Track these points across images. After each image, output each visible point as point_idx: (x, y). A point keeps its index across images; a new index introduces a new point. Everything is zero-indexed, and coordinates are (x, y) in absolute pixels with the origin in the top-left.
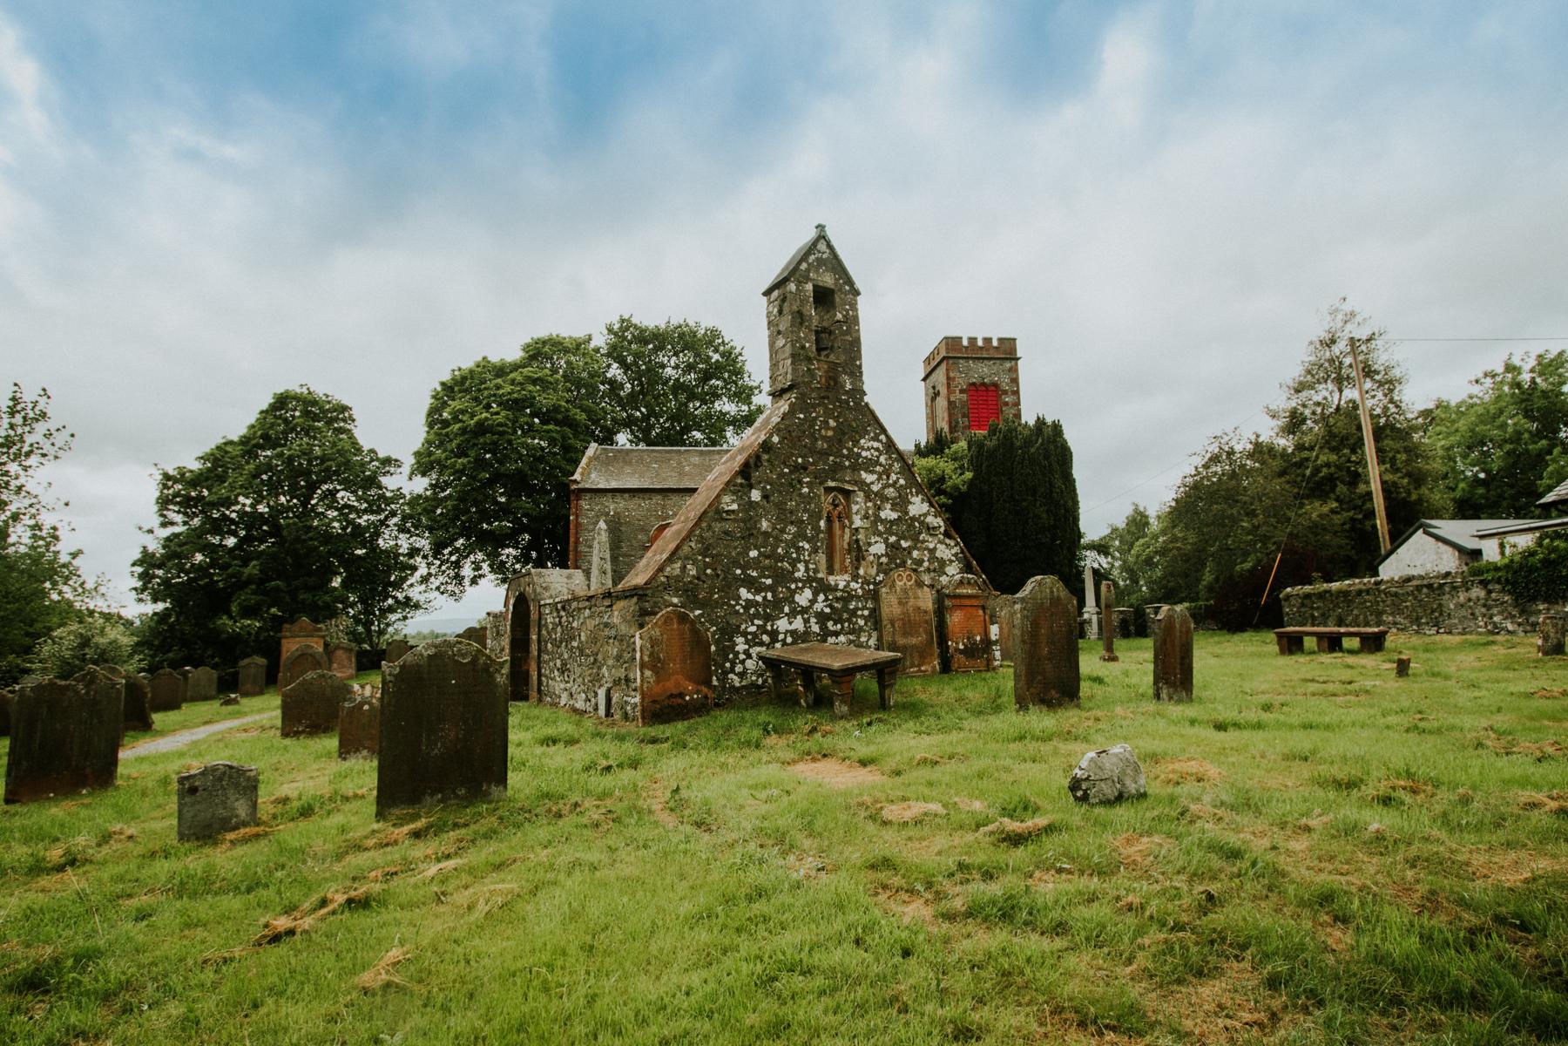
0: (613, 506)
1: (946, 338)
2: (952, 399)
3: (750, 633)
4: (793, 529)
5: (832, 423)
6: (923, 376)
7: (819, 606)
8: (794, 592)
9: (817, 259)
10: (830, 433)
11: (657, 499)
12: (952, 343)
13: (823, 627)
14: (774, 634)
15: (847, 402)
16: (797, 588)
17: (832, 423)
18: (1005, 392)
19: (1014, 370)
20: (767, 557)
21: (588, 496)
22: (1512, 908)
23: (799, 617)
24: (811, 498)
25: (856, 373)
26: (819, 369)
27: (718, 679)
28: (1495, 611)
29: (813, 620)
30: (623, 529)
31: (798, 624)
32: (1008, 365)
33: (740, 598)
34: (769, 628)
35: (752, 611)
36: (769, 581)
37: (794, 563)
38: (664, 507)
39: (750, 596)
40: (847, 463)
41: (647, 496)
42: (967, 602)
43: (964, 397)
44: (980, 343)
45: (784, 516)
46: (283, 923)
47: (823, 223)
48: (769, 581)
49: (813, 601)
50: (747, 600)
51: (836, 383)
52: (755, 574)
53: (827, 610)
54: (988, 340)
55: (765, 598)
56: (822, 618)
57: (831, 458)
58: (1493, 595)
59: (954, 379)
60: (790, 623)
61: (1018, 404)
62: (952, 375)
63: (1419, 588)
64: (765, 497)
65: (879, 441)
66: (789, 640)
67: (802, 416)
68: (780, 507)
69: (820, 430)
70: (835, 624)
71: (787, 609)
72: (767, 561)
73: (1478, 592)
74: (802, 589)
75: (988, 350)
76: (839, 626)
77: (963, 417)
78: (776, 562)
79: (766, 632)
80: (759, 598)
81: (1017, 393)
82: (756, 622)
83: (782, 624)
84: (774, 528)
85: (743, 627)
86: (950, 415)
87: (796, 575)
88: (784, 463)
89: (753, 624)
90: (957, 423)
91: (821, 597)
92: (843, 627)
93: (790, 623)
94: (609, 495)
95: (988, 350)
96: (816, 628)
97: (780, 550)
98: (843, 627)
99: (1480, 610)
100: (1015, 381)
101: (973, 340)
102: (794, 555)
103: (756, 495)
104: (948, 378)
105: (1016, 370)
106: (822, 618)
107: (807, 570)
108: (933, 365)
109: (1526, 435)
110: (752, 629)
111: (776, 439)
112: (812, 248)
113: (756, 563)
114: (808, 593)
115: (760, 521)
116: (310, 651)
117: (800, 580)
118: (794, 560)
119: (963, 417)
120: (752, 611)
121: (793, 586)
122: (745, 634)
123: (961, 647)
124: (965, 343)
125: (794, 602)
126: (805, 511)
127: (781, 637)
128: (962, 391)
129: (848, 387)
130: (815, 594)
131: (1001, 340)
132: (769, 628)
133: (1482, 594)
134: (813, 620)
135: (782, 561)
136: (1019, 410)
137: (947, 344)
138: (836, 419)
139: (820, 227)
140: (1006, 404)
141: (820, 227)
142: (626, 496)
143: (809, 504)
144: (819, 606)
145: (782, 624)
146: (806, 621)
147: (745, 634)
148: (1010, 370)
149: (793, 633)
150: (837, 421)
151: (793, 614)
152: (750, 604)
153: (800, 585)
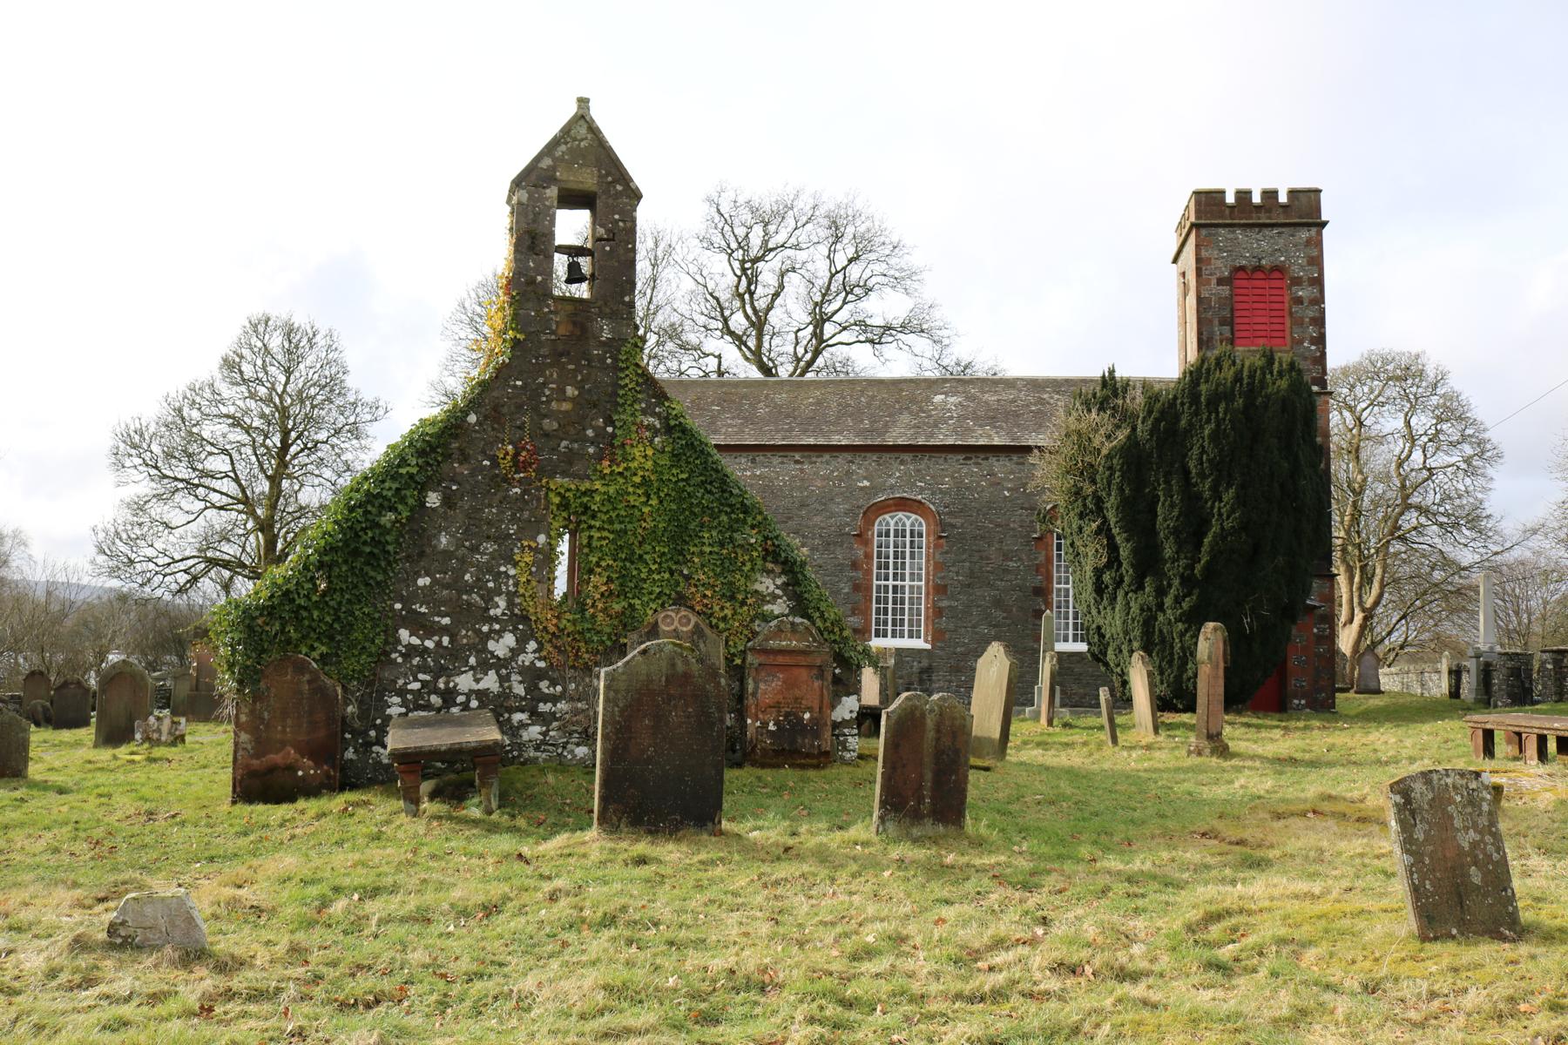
2: (1205, 294)
3: (411, 691)
4: (490, 547)
5: (570, 391)
7: (526, 659)
8: (488, 636)
9: (570, 150)
10: (566, 406)
13: (532, 688)
14: (449, 696)
15: (602, 359)
16: (491, 631)
17: (570, 391)
18: (1297, 281)
20: (447, 586)
23: (492, 673)
24: (526, 502)
26: (555, 313)
27: (356, 751)
29: (515, 677)
31: (490, 682)
32: (1304, 234)
33: (398, 641)
34: (442, 686)
35: (416, 661)
36: (446, 621)
37: (488, 597)
39: (415, 641)
40: (591, 450)
42: (780, 659)
43: (1225, 290)
44: (1256, 199)
45: (475, 530)
47: (585, 95)
48: (446, 621)
49: (515, 652)
50: (409, 646)
51: (584, 329)
52: (423, 610)
53: (541, 664)
54: (1270, 195)
55: (439, 644)
56: (532, 676)
57: (564, 443)
59: (1208, 261)
60: (477, 681)
61: (1319, 300)
64: (448, 501)
65: (654, 414)
66: (474, 704)
67: (519, 383)
68: (473, 516)
69: (549, 402)
70: (553, 683)
71: (472, 661)
72: (445, 592)
74: (500, 633)
75: (1269, 211)
76: (559, 688)
77: (1222, 323)
78: (460, 593)
79: (436, 691)
80: (429, 644)
81: (1319, 282)
82: (421, 676)
83: (465, 682)
84: (460, 545)
85: (401, 682)
87: (492, 612)
88: (483, 452)
89: (416, 679)
90: (1212, 333)
91: (532, 645)
92: (565, 689)
93: (477, 681)
95: (1269, 211)
96: (519, 690)
97: (467, 577)
98: (565, 689)
100: (1317, 262)
101: (1244, 196)
102: (491, 585)
103: (433, 500)
105: (1319, 244)
106: (532, 676)
107: (511, 605)
110: (416, 686)
111: (472, 418)
112: (566, 131)
113: (427, 595)
114: (509, 640)
115: (436, 536)
116: (128, 669)
117: (496, 619)
118: (489, 590)
119: (1222, 323)
120: (416, 661)
121: (485, 629)
122: (402, 692)
123: (772, 727)
124: (1230, 199)
125: (485, 650)
126: (513, 519)
127: (461, 699)
128: (1220, 282)
129: (606, 335)
130: (522, 642)
132: (442, 686)
134: (515, 677)
135: (469, 593)
136: (1323, 312)
138: (579, 386)
139: (583, 102)
140: (1299, 301)
141: (583, 102)
143: (522, 510)
144: (526, 659)
145: (465, 682)
146: (503, 679)
147: (402, 692)
148: (1308, 242)
149: (482, 695)
150: (580, 388)
151: (484, 666)
152: (411, 651)
153: (497, 627)
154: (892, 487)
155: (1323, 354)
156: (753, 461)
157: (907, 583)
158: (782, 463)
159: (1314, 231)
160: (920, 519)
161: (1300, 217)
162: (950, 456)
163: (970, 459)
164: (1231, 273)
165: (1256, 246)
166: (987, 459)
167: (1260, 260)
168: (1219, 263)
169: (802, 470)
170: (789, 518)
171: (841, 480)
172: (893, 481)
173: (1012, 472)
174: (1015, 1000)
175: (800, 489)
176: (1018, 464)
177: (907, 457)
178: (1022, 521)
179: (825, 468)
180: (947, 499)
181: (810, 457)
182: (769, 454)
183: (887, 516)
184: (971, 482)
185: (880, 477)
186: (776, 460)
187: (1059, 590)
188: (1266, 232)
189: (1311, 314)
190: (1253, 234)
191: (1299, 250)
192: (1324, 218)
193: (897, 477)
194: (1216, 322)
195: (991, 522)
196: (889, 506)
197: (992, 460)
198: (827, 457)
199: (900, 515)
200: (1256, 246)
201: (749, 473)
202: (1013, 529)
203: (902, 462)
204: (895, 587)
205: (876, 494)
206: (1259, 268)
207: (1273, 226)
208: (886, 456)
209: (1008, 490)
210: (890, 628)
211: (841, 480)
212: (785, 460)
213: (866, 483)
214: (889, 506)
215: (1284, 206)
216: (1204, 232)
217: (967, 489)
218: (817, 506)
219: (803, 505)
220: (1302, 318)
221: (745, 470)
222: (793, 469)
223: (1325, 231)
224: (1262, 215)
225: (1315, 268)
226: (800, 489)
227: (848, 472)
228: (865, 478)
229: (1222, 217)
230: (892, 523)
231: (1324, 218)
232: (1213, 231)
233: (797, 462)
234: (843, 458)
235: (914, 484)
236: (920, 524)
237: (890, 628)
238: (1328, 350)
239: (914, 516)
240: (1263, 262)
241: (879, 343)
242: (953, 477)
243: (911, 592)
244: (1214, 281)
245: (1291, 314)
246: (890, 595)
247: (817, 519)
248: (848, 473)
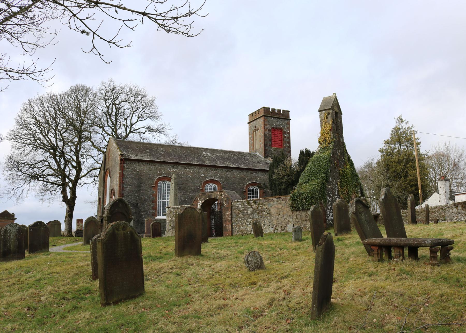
0: (138, 167)
1: (264, 108)
6: (248, 122)
11: (157, 166)
12: (266, 110)
18: (285, 132)
19: (288, 124)
21: (127, 162)
22: (364, 298)
25: (343, 138)
28: (459, 215)
30: (142, 178)
32: (286, 121)
38: (160, 170)
41: (153, 164)
43: (270, 133)
46: (222, 302)
54: (279, 111)
58: (459, 211)
62: (266, 123)
63: (439, 210)
73: (455, 210)
75: (279, 115)
81: (289, 133)
86: (265, 140)
94: (137, 162)
99: (455, 215)
100: (289, 128)
104: (264, 124)
108: (253, 117)
109: (457, 166)
128: (269, 130)
131: (284, 111)
133: (456, 210)
136: (290, 140)
137: (264, 110)
140: (285, 137)
142: (144, 163)
154: (210, 177)
155: (290, 151)
156: (173, 167)
157: (162, 200)
158: (181, 168)
159: (288, 121)
160: (258, 188)
161: (285, 117)
162: (224, 169)
163: (228, 170)
164: (271, 128)
165: (277, 123)
166: (233, 171)
167: (277, 126)
168: (269, 126)
169: (186, 170)
170: (183, 184)
171: (197, 174)
172: (210, 175)
173: (238, 175)
174: (405, 321)
175: (186, 176)
176: (240, 172)
177: (213, 169)
178: (241, 187)
179: (192, 170)
180: (223, 181)
181: (188, 167)
182: (177, 165)
183: (208, 184)
184: (229, 176)
185: (207, 174)
186: (179, 167)
187: (159, 201)
188: (278, 119)
189: (288, 141)
190: (276, 120)
191: (285, 125)
192: (290, 118)
193: (211, 174)
194: (268, 140)
195: (234, 187)
196: (209, 182)
197: (234, 171)
198: (193, 167)
199: (211, 184)
200: (277, 123)
201: (172, 170)
202: (239, 189)
203: (212, 170)
204: (163, 202)
205: (206, 178)
206: (277, 128)
207: (280, 118)
208: (208, 168)
209: (238, 179)
210: (162, 213)
211: (197, 174)
212: (182, 167)
213: (203, 175)
214: (209, 182)
215: (282, 114)
216: (265, 118)
217: (228, 178)
218: (190, 180)
219: (187, 180)
220: (286, 141)
221: (171, 169)
222: (184, 170)
223: (290, 120)
224: (278, 115)
225: (289, 130)
226: (186, 176)
227: (198, 172)
228: (203, 174)
229: (269, 115)
230: (209, 186)
231: (290, 118)
232: (267, 117)
233: (185, 168)
234: (197, 168)
235: (215, 176)
236: (216, 187)
237: (162, 213)
238: (291, 150)
239: (214, 185)
240: (278, 127)
241: (145, 134)
242: (225, 175)
243: (163, 203)
244: (268, 130)
245: (283, 140)
246: (162, 204)
247: (191, 184)
248: (199, 172)
